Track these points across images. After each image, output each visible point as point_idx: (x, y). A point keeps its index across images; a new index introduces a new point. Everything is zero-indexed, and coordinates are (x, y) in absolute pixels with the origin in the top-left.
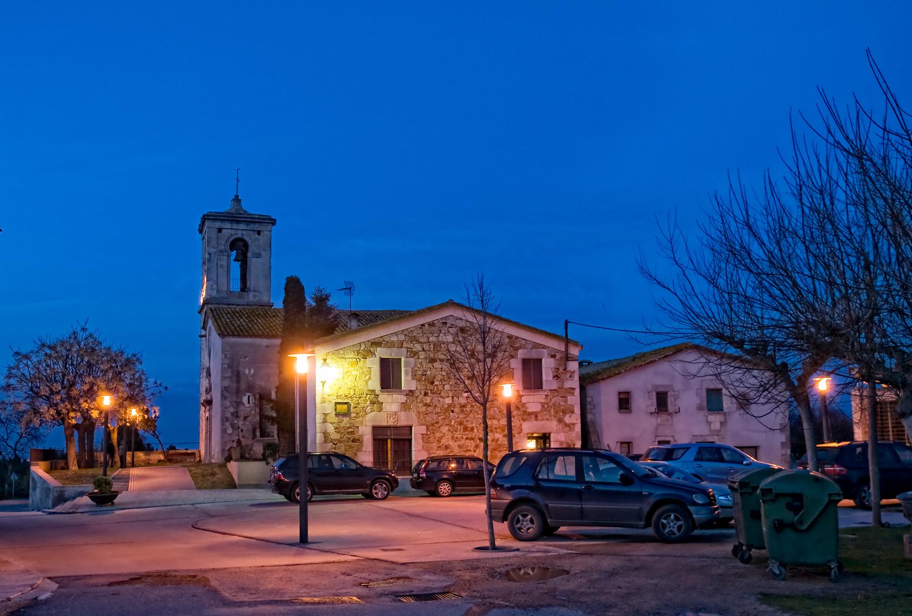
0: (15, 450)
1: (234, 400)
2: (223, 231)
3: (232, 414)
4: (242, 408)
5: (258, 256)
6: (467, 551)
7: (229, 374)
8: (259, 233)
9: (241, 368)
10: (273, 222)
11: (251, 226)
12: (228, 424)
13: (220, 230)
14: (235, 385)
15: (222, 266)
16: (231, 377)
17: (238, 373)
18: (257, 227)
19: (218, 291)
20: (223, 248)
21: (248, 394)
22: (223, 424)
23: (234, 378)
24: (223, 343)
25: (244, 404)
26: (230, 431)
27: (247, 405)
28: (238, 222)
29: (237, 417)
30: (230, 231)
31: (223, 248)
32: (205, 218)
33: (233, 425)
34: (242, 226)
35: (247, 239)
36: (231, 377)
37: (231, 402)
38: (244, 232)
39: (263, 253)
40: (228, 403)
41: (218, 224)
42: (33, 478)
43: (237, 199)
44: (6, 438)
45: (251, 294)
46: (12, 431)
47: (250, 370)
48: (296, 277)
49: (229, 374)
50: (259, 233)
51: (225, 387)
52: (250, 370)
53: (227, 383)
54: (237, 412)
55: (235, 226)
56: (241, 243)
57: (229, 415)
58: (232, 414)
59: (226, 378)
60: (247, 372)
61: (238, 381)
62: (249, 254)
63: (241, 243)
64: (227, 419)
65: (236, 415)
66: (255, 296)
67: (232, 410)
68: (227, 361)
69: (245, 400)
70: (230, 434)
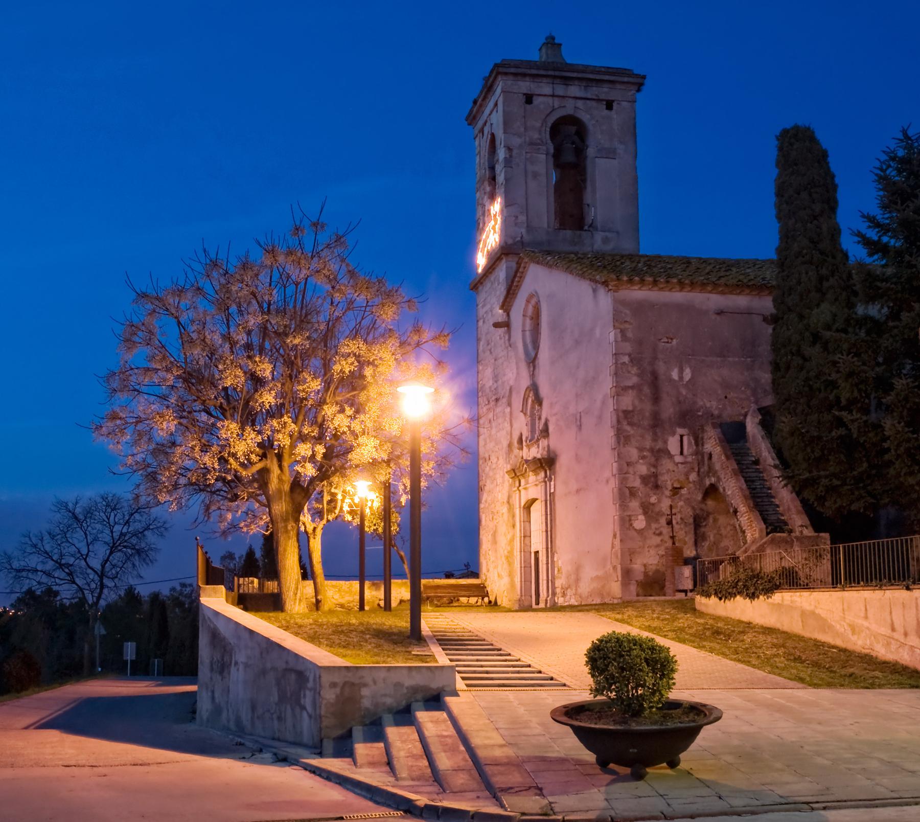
0: (102, 575)
1: (648, 444)
2: (537, 101)
3: (645, 479)
4: (666, 464)
5: (610, 154)
6: (238, 670)
7: (635, 380)
8: (609, 105)
9: (661, 367)
10: (638, 83)
11: (593, 92)
12: (634, 504)
13: (529, 99)
14: (648, 407)
15: (535, 175)
16: (637, 388)
17: (655, 376)
18: (604, 92)
19: (529, 228)
20: (536, 136)
21: (680, 431)
22: (623, 506)
23: (647, 390)
24: (615, 301)
25: (671, 457)
26: (640, 522)
27: (678, 459)
28: (566, 81)
29: (657, 487)
30: (552, 102)
31: (536, 136)
32: (501, 69)
33: (647, 509)
34: (574, 90)
35: (585, 117)
36: (637, 388)
37: (641, 449)
38: (580, 104)
39: (620, 149)
40: (634, 453)
41: (525, 86)
42: (215, 636)
43: (551, 43)
44: (84, 551)
45: (599, 237)
46: (96, 539)
47: (681, 371)
48: (808, 129)
49: (635, 380)
50: (609, 105)
51: (626, 412)
52: (681, 371)
53: (628, 401)
54: (655, 476)
55: (560, 90)
56: (573, 129)
57: (637, 483)
58: (645, 479)
59: (626, 389)
60: (675, 375)
61: (656, 399)
62: (591, 152)
63: (573, 129)
64: (633, 493)
65: (653, 482)
66: (606, 241)
67: (643, 469)
68: (628, 347)
69: (673, 445)
70: (640, 532)
